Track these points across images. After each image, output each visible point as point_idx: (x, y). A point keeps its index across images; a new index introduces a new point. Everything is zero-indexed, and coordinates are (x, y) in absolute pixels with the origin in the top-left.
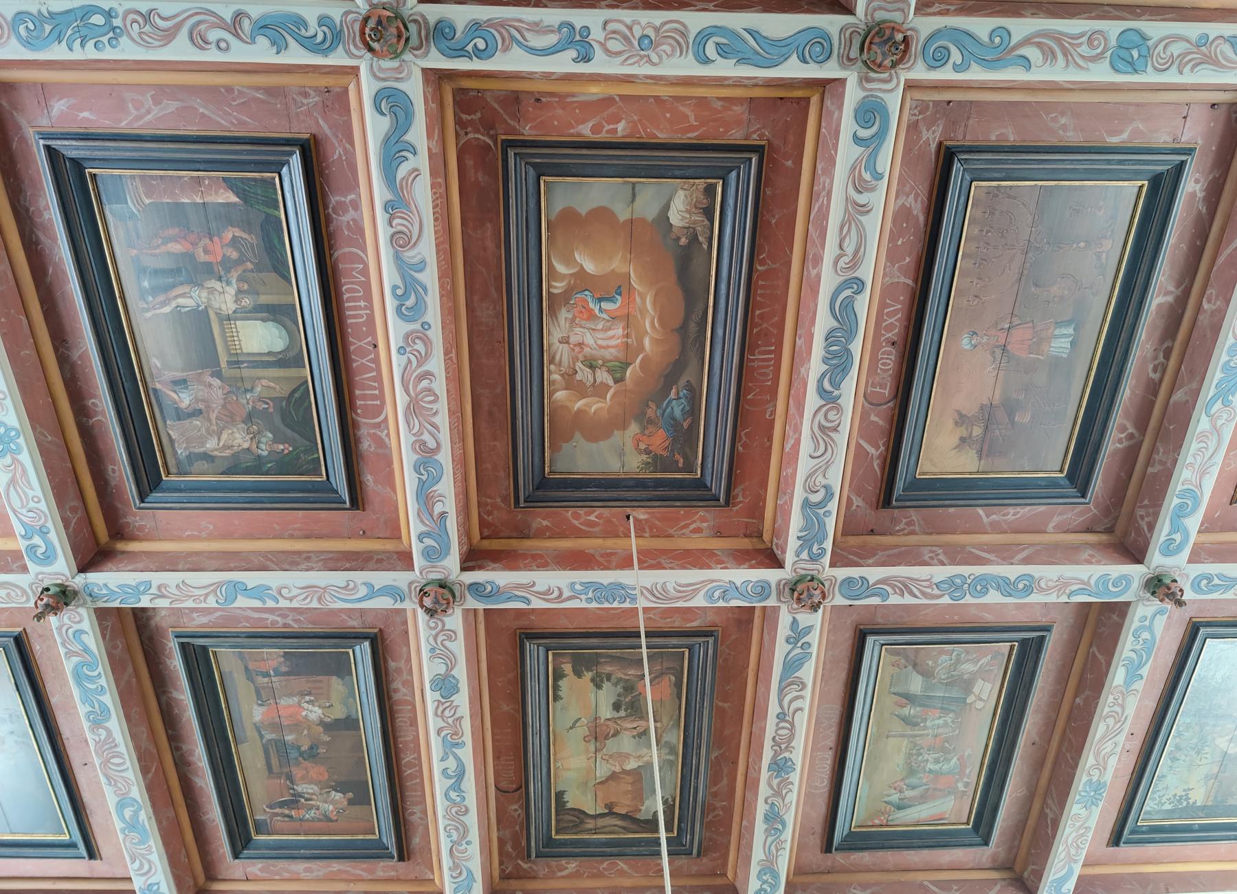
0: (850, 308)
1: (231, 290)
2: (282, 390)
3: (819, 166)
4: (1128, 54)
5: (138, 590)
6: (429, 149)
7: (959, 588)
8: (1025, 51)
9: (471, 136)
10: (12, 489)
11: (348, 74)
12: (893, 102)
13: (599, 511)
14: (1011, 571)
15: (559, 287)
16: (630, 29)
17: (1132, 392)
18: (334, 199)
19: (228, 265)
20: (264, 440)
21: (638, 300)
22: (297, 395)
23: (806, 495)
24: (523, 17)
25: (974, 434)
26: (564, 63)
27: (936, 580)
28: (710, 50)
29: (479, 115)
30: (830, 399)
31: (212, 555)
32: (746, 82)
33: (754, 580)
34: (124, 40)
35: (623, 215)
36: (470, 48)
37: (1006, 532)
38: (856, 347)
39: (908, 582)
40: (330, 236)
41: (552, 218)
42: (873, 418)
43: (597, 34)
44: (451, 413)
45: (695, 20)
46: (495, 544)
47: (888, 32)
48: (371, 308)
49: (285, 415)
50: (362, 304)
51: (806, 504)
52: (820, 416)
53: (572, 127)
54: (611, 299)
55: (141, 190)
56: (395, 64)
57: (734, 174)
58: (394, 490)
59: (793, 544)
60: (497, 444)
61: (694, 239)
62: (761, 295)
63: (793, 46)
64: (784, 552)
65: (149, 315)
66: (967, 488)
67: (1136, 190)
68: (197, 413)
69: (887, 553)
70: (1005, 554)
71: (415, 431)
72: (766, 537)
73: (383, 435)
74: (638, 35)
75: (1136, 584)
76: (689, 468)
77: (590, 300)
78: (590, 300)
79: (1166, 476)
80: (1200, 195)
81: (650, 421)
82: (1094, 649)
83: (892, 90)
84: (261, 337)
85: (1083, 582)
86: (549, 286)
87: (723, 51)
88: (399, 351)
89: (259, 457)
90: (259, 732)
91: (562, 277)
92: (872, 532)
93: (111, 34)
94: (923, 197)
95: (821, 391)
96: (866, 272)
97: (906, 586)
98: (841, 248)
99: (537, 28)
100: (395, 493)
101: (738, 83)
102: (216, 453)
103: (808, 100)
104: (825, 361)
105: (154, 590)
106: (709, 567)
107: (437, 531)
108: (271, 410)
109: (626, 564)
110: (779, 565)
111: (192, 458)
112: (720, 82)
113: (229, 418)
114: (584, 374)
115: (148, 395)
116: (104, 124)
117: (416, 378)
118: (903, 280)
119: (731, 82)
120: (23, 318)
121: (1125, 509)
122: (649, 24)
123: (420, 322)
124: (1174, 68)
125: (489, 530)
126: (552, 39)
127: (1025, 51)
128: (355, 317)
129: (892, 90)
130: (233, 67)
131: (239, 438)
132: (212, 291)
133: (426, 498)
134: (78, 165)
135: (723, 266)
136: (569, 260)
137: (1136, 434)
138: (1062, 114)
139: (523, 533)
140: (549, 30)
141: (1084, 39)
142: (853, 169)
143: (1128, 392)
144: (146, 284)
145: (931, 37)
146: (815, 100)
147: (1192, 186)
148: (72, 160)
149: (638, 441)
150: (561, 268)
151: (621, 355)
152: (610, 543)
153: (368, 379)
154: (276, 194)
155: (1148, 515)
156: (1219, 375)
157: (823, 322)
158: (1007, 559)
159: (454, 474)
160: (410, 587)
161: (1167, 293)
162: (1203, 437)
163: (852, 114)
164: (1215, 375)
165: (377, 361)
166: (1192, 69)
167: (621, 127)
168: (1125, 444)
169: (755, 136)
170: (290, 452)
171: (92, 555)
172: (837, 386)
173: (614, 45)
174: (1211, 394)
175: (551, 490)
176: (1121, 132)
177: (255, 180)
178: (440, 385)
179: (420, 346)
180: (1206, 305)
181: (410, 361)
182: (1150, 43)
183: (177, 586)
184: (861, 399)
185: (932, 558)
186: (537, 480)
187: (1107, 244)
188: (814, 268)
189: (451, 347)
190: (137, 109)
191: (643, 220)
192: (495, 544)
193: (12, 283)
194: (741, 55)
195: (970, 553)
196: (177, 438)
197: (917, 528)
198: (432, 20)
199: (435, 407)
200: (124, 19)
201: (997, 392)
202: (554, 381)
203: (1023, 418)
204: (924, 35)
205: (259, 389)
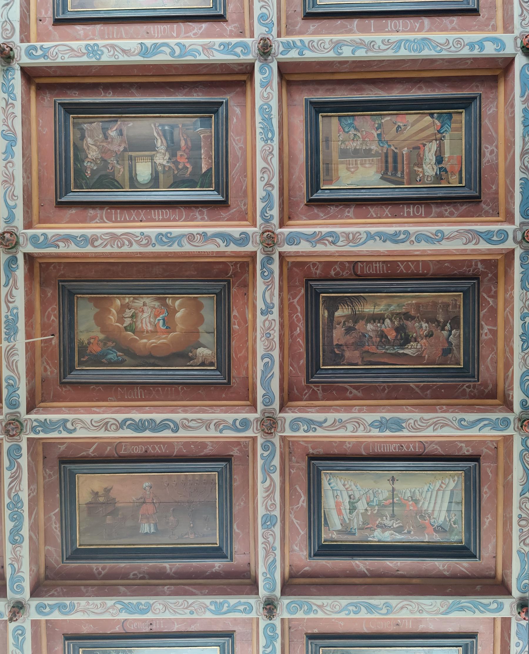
0: (165, 428)
1: (165, 163)
2: (118, 177)
3: (223, 408)
4: (269, 520)
6: (227, 252)
7: (15, 506)
9: (231, 267)
10: (69, 48)
11: (253, 222)
12: (249, 433)
13: (57, 321)
14: (25, 531)
15: (169, 302)
16: (273, 329)
17: (122, 568)
18: (205, 210)
19: (176, 163)
20: (92, 165)
21: (164, 336)
22: (116, 183)
23: (71, 420)
24: (276, 290)
25: (99, 498)
26: (260, 305)
27: (20, 493)
28: (266, 360)
29: (239, 271)
30: (122, 425)
33: (20, 400)
34: (263, 143)
35: (201, 329)
36: (264, 270)
37: (45, 525)
38: (147, 434)
40: (190, 208)
41: (199, 299)
42: (109, 448)
43: (271, 317)
44: (111, 253)
45: (276, 353)
46: (37, 270)
47: (274, 426)
48: (159, 221)
49: (106, 176)
51: (66, 421)
52: (113, 422)
53: (236, 308)
54: (164, 324)
55: (206, 134)
56: (258, 241)
57: (219, 373)
59: (42, 417)
60: (93, 273)
62: (168, 389)
64: (36, 413)
65: (153, 126)
67: (215, 542)
68: (106, 137)
69: (34, 466)
70: (34, 527)
71: (103, 236)
72: (42, 404)
73: (97, 220)
74: (270, 332)
75: (18, 597)
76: (80, 363)
79: (81, 595)
80: (214, 570)
81: (105, 344)
84: (144, 171)
85: (19, 569)
86: (169, 298)
89: (84, 161)
91: (173, 303)
92: (45, 457)
93: (265, 139)
94: (211, 453)
95: (125, 421)
96: (182, 433)
97: (16, 478)
98: (192, 420)
99: (272, 295)
101: (254, 372)
102: (85, 142)
103: (248, 400)
104: (141, 420)
105: (10, 101)
106: (27, 377)
107: (48, 243)
108: (108, 171)
109: (28, 336)
112: (255, 364)
113: (103, 151)
114: (128, 313)
115: (114, 117)
116: (231, 127)
117: (130, 239)
118: (176, 450)
119: (254, 369)
120: (151, 74)
121: (59, 582)
124: (264, 540)
126: (269, 301)
128: (155, 214)
129: (253, 431)
130: (254, 181)
131: (93, 153)
132: (165, 155)
133: (67, 239)
134: (216, 112)
135: (179, 372)
136: (181, 306)
137: (101, 576)
138: (245, 503)
139: (44, 283)
140: (271, 299)
142: (224, 421)
143: (123, 565)
144: (166, 128)
146: (248, 403)
147: (217, 564)
148: (218, 110)
149: (95, 339)
150: (177, 303)
151: (138, 329)
153: (125, 216)
154: (206, 188)
155: (58, 593)
156: (135, 602)
157: (158, 417)
158: (31, 529)
159: (79, 253)
160: (14, 227)
161: (171, 569)
162: (103, 605)
163: (245, 417)
165: (134, 221)
167: (237, 327)
169: (234, 381)
170: (86, 176)
172: (128, 427)
174: (126, 602)
175: (68, 299)
176: (238, 529)
178: (126, 249)
179: (144, 242)
180: (166, 587)
181: (137, 237)
182: (273, 528)
183: (13, 113)
184: (118, 441)
185: (31, 490)
186: (72, 291)
187: (192, 536)
188: (182, 411)
189: (142, 255)
190: (237, 140)
192: (37, 270)
194: (265, 372)
197: (47, 480)
198: (273, 256)
199: (115, 246)
200: (270, 145)
202: (125, 299)
203: (109, 520)
204: (273, 440)
205: (119, 167)
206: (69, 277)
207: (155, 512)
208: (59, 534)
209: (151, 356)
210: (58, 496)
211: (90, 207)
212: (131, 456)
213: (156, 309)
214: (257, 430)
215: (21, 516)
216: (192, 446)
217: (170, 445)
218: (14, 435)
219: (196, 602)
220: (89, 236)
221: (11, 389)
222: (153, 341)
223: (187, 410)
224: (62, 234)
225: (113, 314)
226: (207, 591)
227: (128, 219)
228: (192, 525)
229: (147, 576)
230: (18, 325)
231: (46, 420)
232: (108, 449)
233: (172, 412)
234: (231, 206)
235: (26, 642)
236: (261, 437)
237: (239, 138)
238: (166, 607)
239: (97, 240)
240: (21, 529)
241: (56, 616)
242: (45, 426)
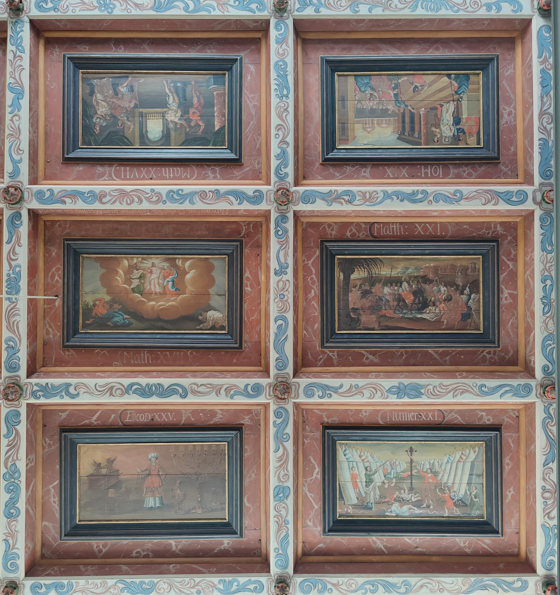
0: (173, 393)
1: (176, 120)
2: (128, 133)
3: (234, 373)
4: (281, 491)
5: (19, 46)
6: (240, 210)
7: (12, 476)
8: (281, 449)
9: (244, 227)
12: (261, 400)
13: (61, 281)
15: (179, 263)
16: (287, 290)
18: (217, 169)
19: (188, 121)
20: (102, 121)
21: (173, 298)
22: (125, 140)
23: (74, 384)
25: (102, 470)
26: (274, 265)
27: (18, 463)
28: (280, 322)
29: (252, 231)
30: (127, 390)
31: (37, 85)
32: (267, 339)
34: (278, 100)
35: (212, 291)
36: (279, 228)
37: (43, 499)
38: (154, 399)
39: (16, 447)
40: (202, 166)
41: (210, 260)
42: (113, 416)
43: (285, 277)
47: (288, 391)
48: (170, 179)
49: (115, 133)
50: (172, 175)
51: (68, 385)
54: (173, 286)
56: (272, 199)
57: (230, 337)
58: (73, 180)
59: (43, 381)
60: (100, 232)
61: (201, 322)
62: (176, 354)
63: (282, 355)
64: (36, 378)
66: (71, 473)
68: (116, 93)
70: (31, 501)
71: (111, 192)
72: (43, 369)
73: (105, 178)
76: (85, 326)
77: (173, 276)
78: (173, 276)
80: (222, 547)
81: (111, 306)
83: (266, 397)
84: (154, 128)
85: (14, 545)
87: (280, 327)
88: (152, 189)
89: (93, 117)
91: (183, 264)
94: (221, 421)
95: (132, 385)
97: (14, 447)
99: (286, 255)
100: (72, 180)
101: (267, 336)
104: (148, 385)
106: (28, 338)
107: (54, 199)
109: (30, 293)
110: (28, 376)
111: (92, 86)
112: (267, 328)
113: (113, 107)
114: (136, 274)
115: (125, 73)
116: (245, 85)
118: (184, 419)
120: (164, 29)
122: (288, 298)
123: (167, 200)
124: (276, 513)
125: (50, 225)
126: (282, 260)
127: (281, 449)
128: (165, 171)
130: (269, 138)
131: (102, 109)
132: (176, 112)
133: (74, 195)
134: (230, 69)
135: (190, 335)
136: (191, 267)
138: (256, 475)
140: (286, 259)
141: (286, 472)
142: (235, 386)
143: (125, 542)
144: (179, 85)
145: (286, 410)
146: (261, 368)
148: (232, 68)
150: (188, 264)
151: (146, 291)
152: (41, 287)
160: (19, 182)
161: (177, 546)
162: (104, 584)
164: (137, 579)
165: (144, 179)
166: (277, 522)
167: (249, 289)
168: (96, 550)
169: (246, 345)
170: (95, 132)
171: (38, 28)
173: (281, 284)
177: (225, 138)
178: (135, 206)
179: (155, 199)
180: (171, 566)
181: (147, 194)
182: (285, 500)
183: (21, 66)
185: (29, 460)
186: (77, 250)
190: (251, 98)
191: (209, 299)
193: (180, 29)
194: (278, 334)
195: (32, 480)
196: (103, 83)
198: (288, 215)
199: (124, 203)
201: (125, 477)
203: (111, 493)
204: (286, 407)
205: (129, 123)
207: (161, 484)
208: (58, 508)
209: (159, 319)
210: (58, 467)
213: (165, 270)
214: (269, 396)
215: (18, 487)
216: (201, 414)
222: (162, 304)
223: (196, 375)
224: (69, 190)
225: (120, 274)
228: (199, 499)
230: (20, 284)
231: (47, 384)
232: (112, 417)
233: (181, 377)
236: (274, 403)
239: (105, 196)
240: (17, 501)
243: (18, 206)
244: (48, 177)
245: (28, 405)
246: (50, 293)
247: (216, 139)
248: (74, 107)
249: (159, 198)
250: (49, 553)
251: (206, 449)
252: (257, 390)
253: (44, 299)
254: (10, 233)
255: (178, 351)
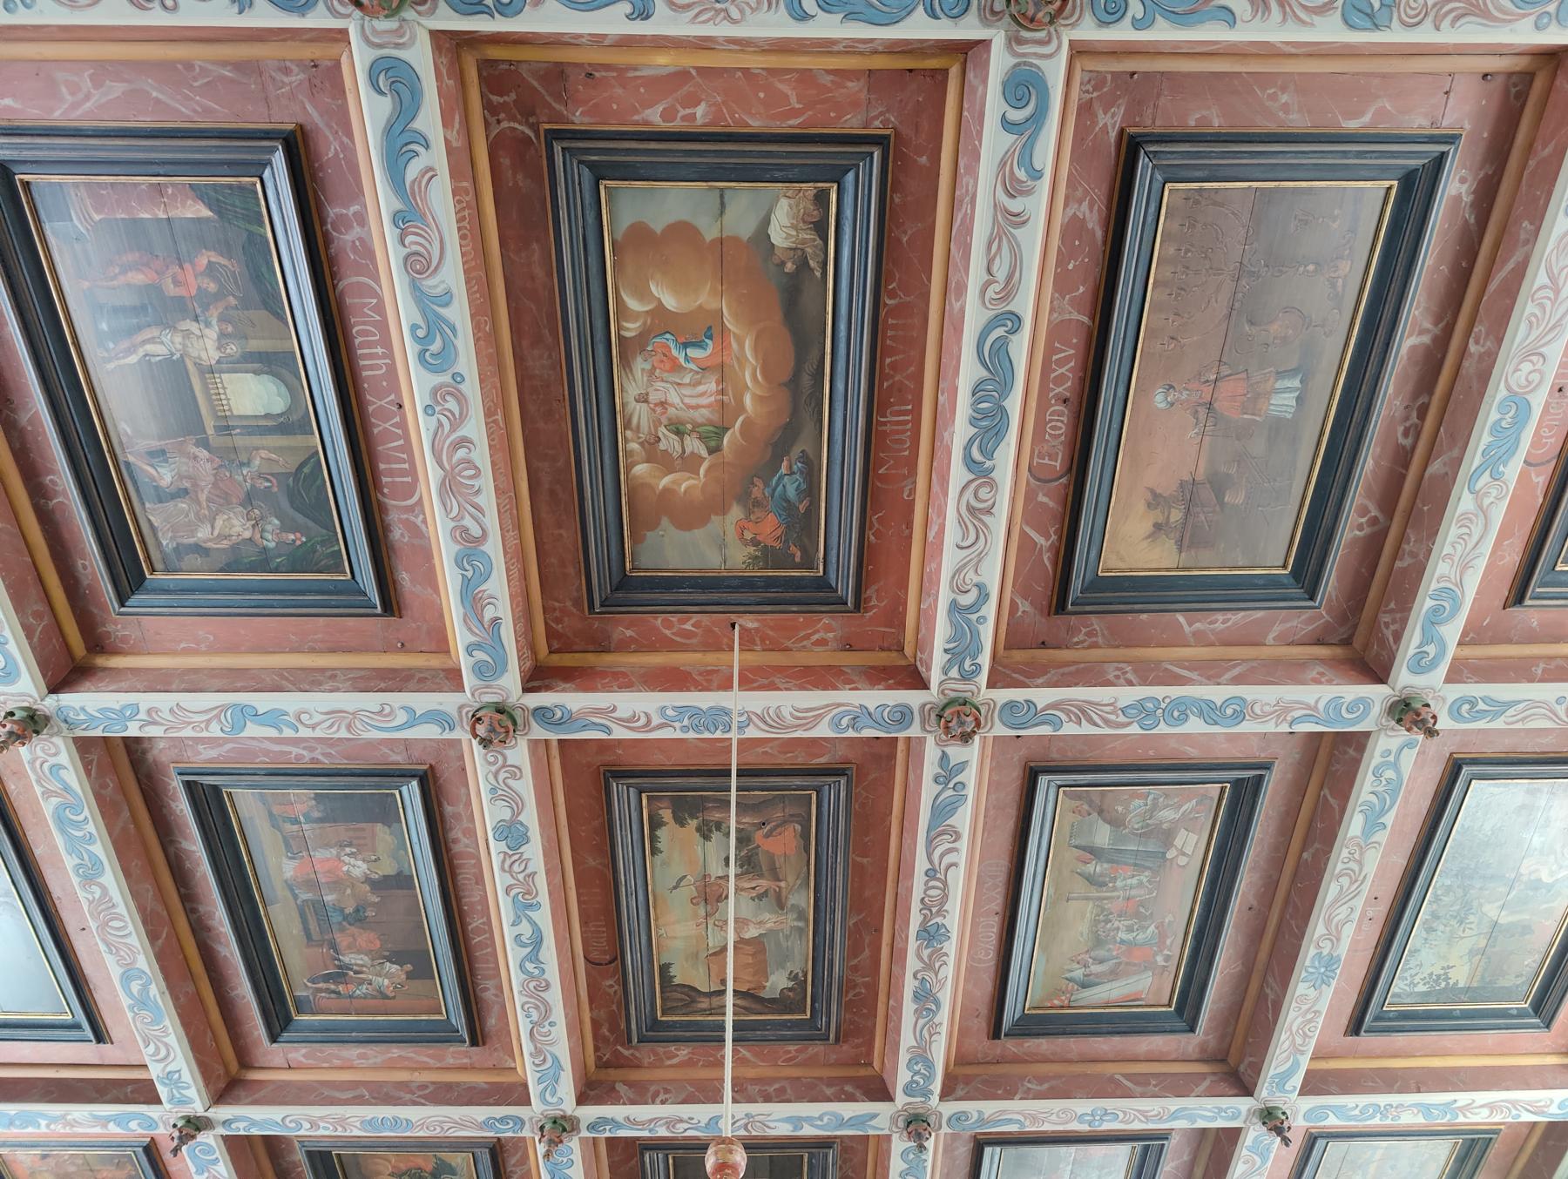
0: (1003, 351)
1: (212, 333)
2: (289, 464)
3: (961, 164)
5: (122, 715)
9: (505, 124)
12: (1055, 71)
13: (696, 618)
14: (1217, 693)
17: (1376, 463)
18: (332, 212)
19: (206, 300)
21: (734, 345)
22: (306, 470)
23: (953, 596)
27: (1121, 704)
29: (513, 96)
30: (980, 472)
31: (213, 673)
32: (862, 47)
35: (711, 234)
37: (1212, 645)
38: (1014, 404)
40: (332, 261)
41: (619, 237)
42: (1042, 498)
46: (567, 660)
50: (379, 350)
51: (954, 607)
53: (636, 112)
54: (699, 345)
56: (391, 24)
57: (850, 176)
59: (938, 658)
60: (562, 531)
61: (803, 264)
64: (929, 669)
65: (111, 366)
67: (1382, 193)
70: (1211, 672)
72: (908, 650)
73: (419, 521)
75: (1376, 710)
76: (808, 564)
77: (672, 345)
78: (672, 345)
79: (1418, 571)
80: (1467, 199)
81: (757, 503)
82: (1326, 791)
84: (254, 395)
85: (1308, 707)
86: (619, 329)
90: (292, 890)
91: (635, 316)
92: (1043, 645)
94: (1101, 205)
95: (969, 462)
97: (1083, 712)
98: (989, 272)
101: (852, 48)
102: (210, 545)
104: (973, 422)
105: (142, 716)
106: (835, 688)
109: (726, 686)
112: (825, 47)
113: (222, 499)
114: (669, 442)
117: (450, 445)
118: (1075, 316)
119: (840, 47)
124: (1428, 23)
128: (371, 367)
129: (1050, 56)
131: (236, 526)
132: (187, 334)
133: (474, 601)
135: (844, 298)
136: (643, 293)
137: (1381, 517)
138: (1284, 89)
142: (1002, 164)
143: (1370, 463)
146: (954, 71)
149: (743, 529)
150: (633, 304)
151: (715, 417)
152: (711, 658)
153: (395, 449)
155: (1394, 621)
156: (1486, 439)
157: (969, 372)
162: (1466, 520)
163: (999, 88)
167: (700, 111)
168: (1367, 530)
169: (877, 123)
176: (1362, 114)
178: (481, 455)
179: (452, 404)
180: (1472, 348)
181: (440, 424)
184: (1025, 473)
185: (1117, 677)
186: (615, 582)
187: (1345, 267)
188: (957, 300)
190: (73, 94)
191: (736, 239)
192: (567, 660)
194: (849, 8)
196: (163, 525)
197: (1100, 640)
199: (476, 483)
201: (1202, 465)
203: (1235, 498)
205: (257, 462)
206: (579, 589)
207: (1244, 375)
208: (1242, 613)
209: (793, 383)
210: (1144, 616)
211: (386, 537)
212: (1072, 445)
213: (654, 368)
214: (1047, 42)
215: (1178, 702)
216: (1071, 267)
217: (1057, 332)
218: (977, 720)
219: (1549, 262)
220: (457, 547)
221: (866, 720)
222: (750, 376)
223: (958, 283)
224: (462, 611)
225: (674, 482)
226: (1525, 224)
227: (401, 442)
228: (1311, 267)
229: (1423, 399)
230: (704, 707)
231: (946, 651)
232: (1045, 500)
233: (959, 331)
234: (300, 121)
235: (1494, 695)
236: (1073, 25)
237: (64, 90)
238: (1533, 353)
239: (466, 530)
240: (1209, 703)
241: (1452, 632)
242: (956, 655)
243: (518, 715)
244: (442, 644)
245: (991, 684)
246: (725, 640)
247: (242, 212)
248: (250, 592)
249: (449, 393)
250: (1342, 630)
251: (1172, 251)
252: (1025, 86)
253: (741, 650)
254: (584, 727)
255: (884, 333)
